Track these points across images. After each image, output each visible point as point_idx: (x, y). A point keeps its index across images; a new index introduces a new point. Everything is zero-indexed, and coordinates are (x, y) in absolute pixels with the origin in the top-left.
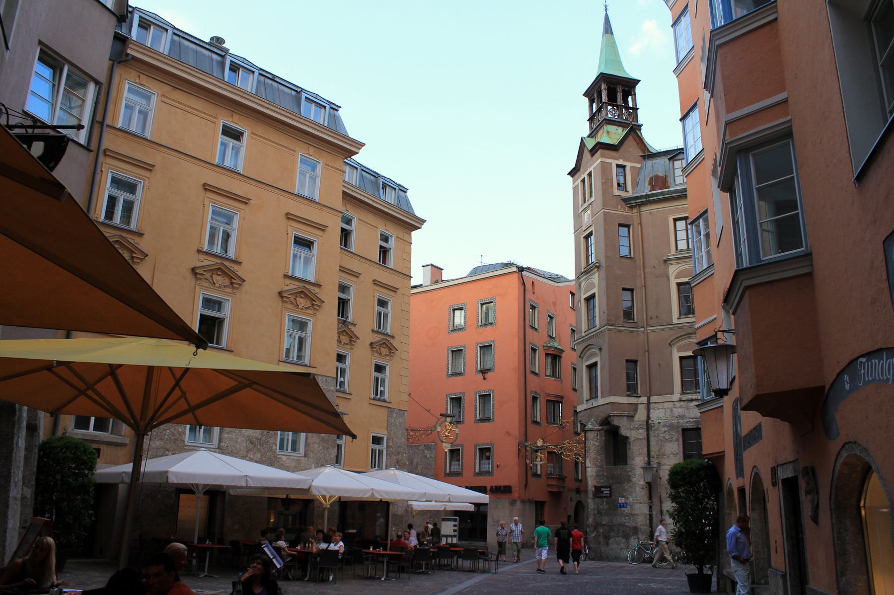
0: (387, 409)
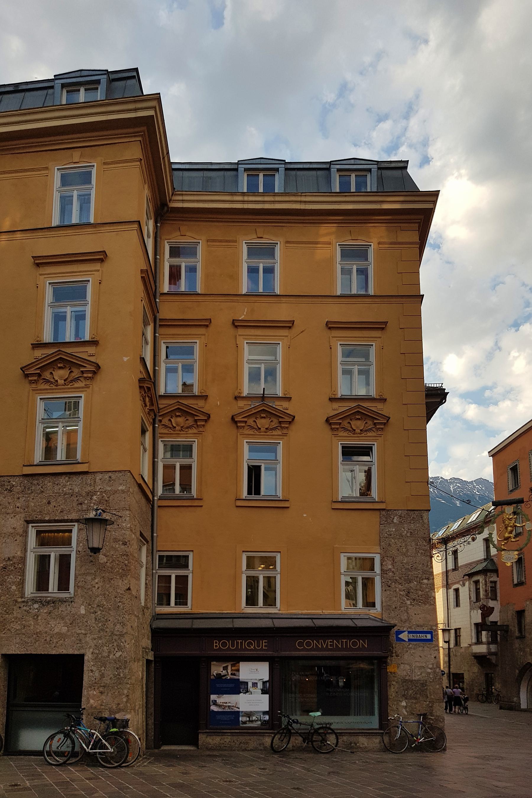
0: (378, 513)
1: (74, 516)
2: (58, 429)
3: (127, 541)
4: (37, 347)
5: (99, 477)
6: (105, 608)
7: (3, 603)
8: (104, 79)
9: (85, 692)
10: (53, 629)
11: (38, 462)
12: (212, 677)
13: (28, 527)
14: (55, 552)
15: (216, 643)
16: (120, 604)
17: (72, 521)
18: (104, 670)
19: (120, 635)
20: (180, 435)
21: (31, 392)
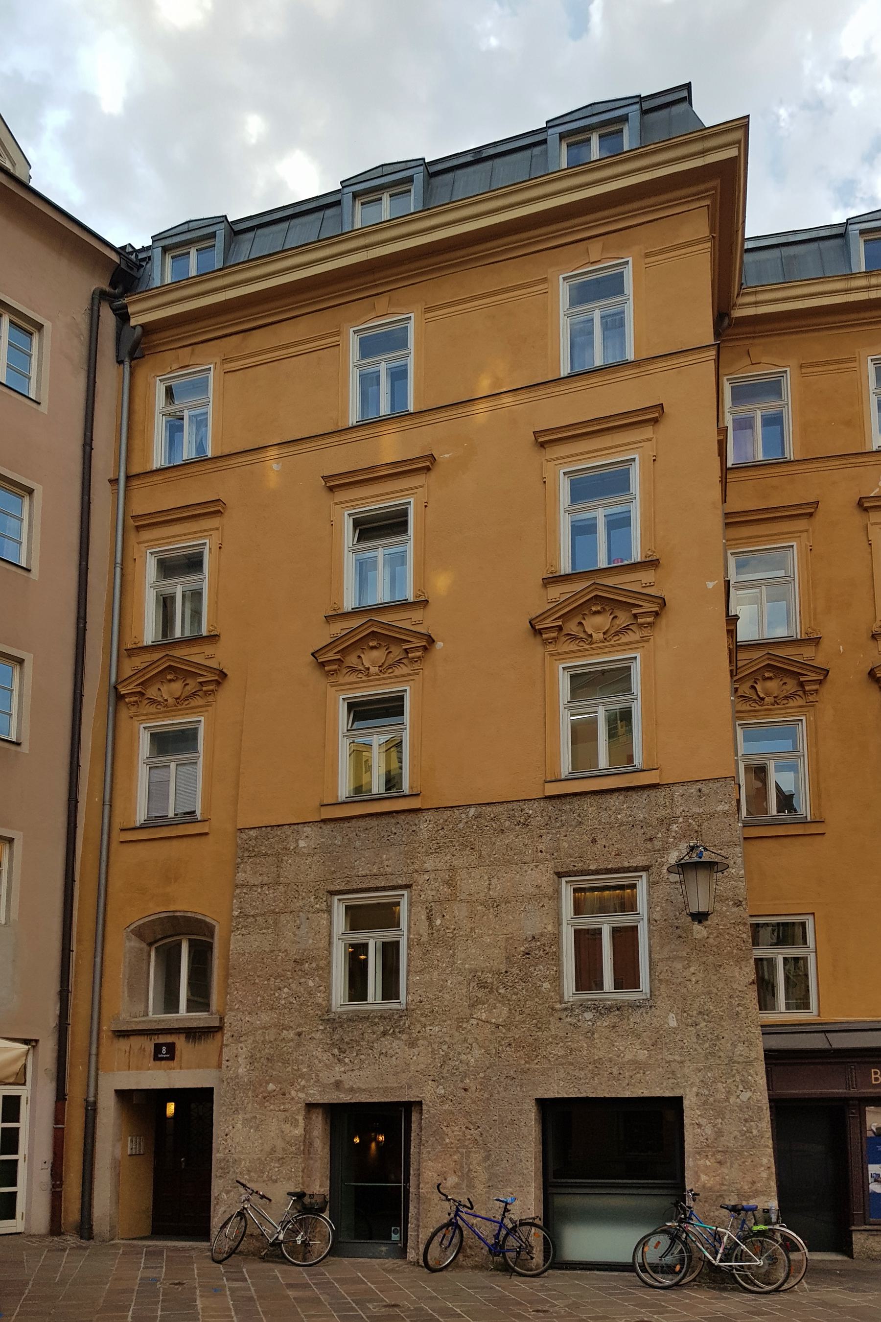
1: (640, 860)
2: (572, 718)
3: (741, 899)
4: (552, 582)
5: (678, 791)
6: (713, 1017)
7: (530, 1012)
8: (634, 111)
9: (689, 1162)
10: (622, 1055)
11: (567, 773)
12: (870, 1134)
13: (560, 884)
14: (608, 923)
15: (876, 1073)
16: (740, 1008)
17: (636, 869)
18: (721, 1123)
19: (746, 1062)
20: (772, 712)
21: (548, 658)
